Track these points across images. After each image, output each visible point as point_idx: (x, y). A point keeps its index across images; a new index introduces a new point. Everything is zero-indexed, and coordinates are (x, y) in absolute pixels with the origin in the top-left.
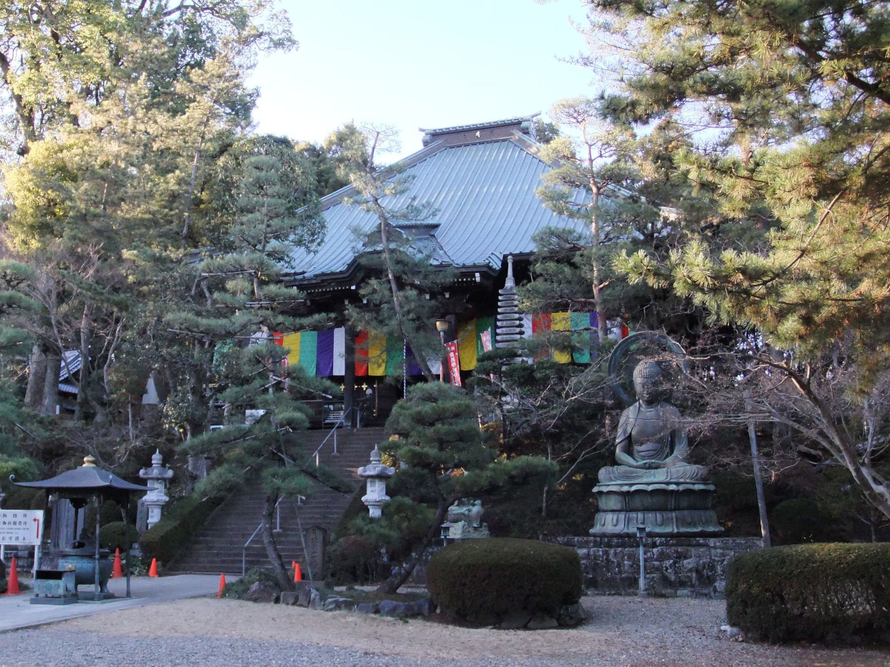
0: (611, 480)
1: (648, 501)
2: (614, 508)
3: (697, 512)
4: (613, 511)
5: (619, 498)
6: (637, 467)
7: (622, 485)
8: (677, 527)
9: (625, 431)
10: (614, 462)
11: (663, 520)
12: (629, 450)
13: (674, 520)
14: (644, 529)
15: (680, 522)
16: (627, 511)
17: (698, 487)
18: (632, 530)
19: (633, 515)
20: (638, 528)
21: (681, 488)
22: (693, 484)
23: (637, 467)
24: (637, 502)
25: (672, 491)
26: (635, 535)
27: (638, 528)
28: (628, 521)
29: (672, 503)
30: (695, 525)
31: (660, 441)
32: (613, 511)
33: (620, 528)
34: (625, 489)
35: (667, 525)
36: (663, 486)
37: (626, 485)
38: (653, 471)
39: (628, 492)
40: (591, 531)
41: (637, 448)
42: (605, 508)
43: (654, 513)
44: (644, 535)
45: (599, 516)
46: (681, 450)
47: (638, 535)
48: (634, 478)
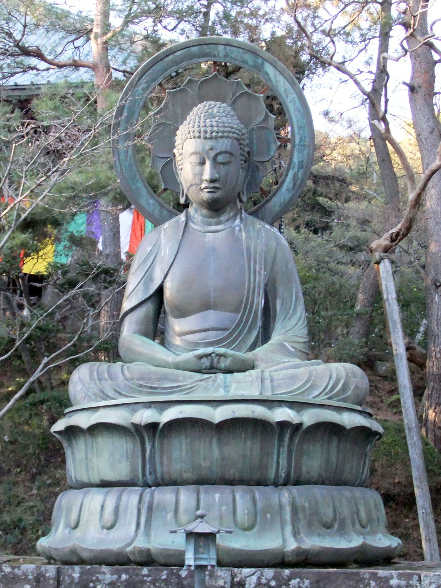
0: (107, 397)
1: (211, 454)
2: (111, 476)
3: (346, 492)
4: (105, 484)
6: (177, 366)
7: (133, 406)
8: (296, 534)
9: (148, 277)
10: (111, 351)
11: (255, 514)
12: (156, 330)
13: (288, 516)
14: (210, 537)
15: (306, 518)
16: (146, 485)
17: (350, 420)
18: (165, 539)
19: (165, 496)
21: (308, 417)
22: (339, 409)
23: (177, 366)
24: (179, 455)
25: (283, 425)
26: (175, 561)
27: (190, 535)
28: (150, 513)
29: (279, 462)
30: (342, 530)
31: (240, 306)
32: (105, 484)
33: (124, 537)
34: (145, 416)
35: (267, 526)
36: (258, 411)
37: (149, 405)
38: (221, 376)
39: (153, 427)
40: (43, 543)
41: (177, 325)
42: (85, 479)
43: (227, 489)
44: (209, 559)
45: (67, 502)
46: (291, 327)
47: (190, 560)
48: (172, 390)
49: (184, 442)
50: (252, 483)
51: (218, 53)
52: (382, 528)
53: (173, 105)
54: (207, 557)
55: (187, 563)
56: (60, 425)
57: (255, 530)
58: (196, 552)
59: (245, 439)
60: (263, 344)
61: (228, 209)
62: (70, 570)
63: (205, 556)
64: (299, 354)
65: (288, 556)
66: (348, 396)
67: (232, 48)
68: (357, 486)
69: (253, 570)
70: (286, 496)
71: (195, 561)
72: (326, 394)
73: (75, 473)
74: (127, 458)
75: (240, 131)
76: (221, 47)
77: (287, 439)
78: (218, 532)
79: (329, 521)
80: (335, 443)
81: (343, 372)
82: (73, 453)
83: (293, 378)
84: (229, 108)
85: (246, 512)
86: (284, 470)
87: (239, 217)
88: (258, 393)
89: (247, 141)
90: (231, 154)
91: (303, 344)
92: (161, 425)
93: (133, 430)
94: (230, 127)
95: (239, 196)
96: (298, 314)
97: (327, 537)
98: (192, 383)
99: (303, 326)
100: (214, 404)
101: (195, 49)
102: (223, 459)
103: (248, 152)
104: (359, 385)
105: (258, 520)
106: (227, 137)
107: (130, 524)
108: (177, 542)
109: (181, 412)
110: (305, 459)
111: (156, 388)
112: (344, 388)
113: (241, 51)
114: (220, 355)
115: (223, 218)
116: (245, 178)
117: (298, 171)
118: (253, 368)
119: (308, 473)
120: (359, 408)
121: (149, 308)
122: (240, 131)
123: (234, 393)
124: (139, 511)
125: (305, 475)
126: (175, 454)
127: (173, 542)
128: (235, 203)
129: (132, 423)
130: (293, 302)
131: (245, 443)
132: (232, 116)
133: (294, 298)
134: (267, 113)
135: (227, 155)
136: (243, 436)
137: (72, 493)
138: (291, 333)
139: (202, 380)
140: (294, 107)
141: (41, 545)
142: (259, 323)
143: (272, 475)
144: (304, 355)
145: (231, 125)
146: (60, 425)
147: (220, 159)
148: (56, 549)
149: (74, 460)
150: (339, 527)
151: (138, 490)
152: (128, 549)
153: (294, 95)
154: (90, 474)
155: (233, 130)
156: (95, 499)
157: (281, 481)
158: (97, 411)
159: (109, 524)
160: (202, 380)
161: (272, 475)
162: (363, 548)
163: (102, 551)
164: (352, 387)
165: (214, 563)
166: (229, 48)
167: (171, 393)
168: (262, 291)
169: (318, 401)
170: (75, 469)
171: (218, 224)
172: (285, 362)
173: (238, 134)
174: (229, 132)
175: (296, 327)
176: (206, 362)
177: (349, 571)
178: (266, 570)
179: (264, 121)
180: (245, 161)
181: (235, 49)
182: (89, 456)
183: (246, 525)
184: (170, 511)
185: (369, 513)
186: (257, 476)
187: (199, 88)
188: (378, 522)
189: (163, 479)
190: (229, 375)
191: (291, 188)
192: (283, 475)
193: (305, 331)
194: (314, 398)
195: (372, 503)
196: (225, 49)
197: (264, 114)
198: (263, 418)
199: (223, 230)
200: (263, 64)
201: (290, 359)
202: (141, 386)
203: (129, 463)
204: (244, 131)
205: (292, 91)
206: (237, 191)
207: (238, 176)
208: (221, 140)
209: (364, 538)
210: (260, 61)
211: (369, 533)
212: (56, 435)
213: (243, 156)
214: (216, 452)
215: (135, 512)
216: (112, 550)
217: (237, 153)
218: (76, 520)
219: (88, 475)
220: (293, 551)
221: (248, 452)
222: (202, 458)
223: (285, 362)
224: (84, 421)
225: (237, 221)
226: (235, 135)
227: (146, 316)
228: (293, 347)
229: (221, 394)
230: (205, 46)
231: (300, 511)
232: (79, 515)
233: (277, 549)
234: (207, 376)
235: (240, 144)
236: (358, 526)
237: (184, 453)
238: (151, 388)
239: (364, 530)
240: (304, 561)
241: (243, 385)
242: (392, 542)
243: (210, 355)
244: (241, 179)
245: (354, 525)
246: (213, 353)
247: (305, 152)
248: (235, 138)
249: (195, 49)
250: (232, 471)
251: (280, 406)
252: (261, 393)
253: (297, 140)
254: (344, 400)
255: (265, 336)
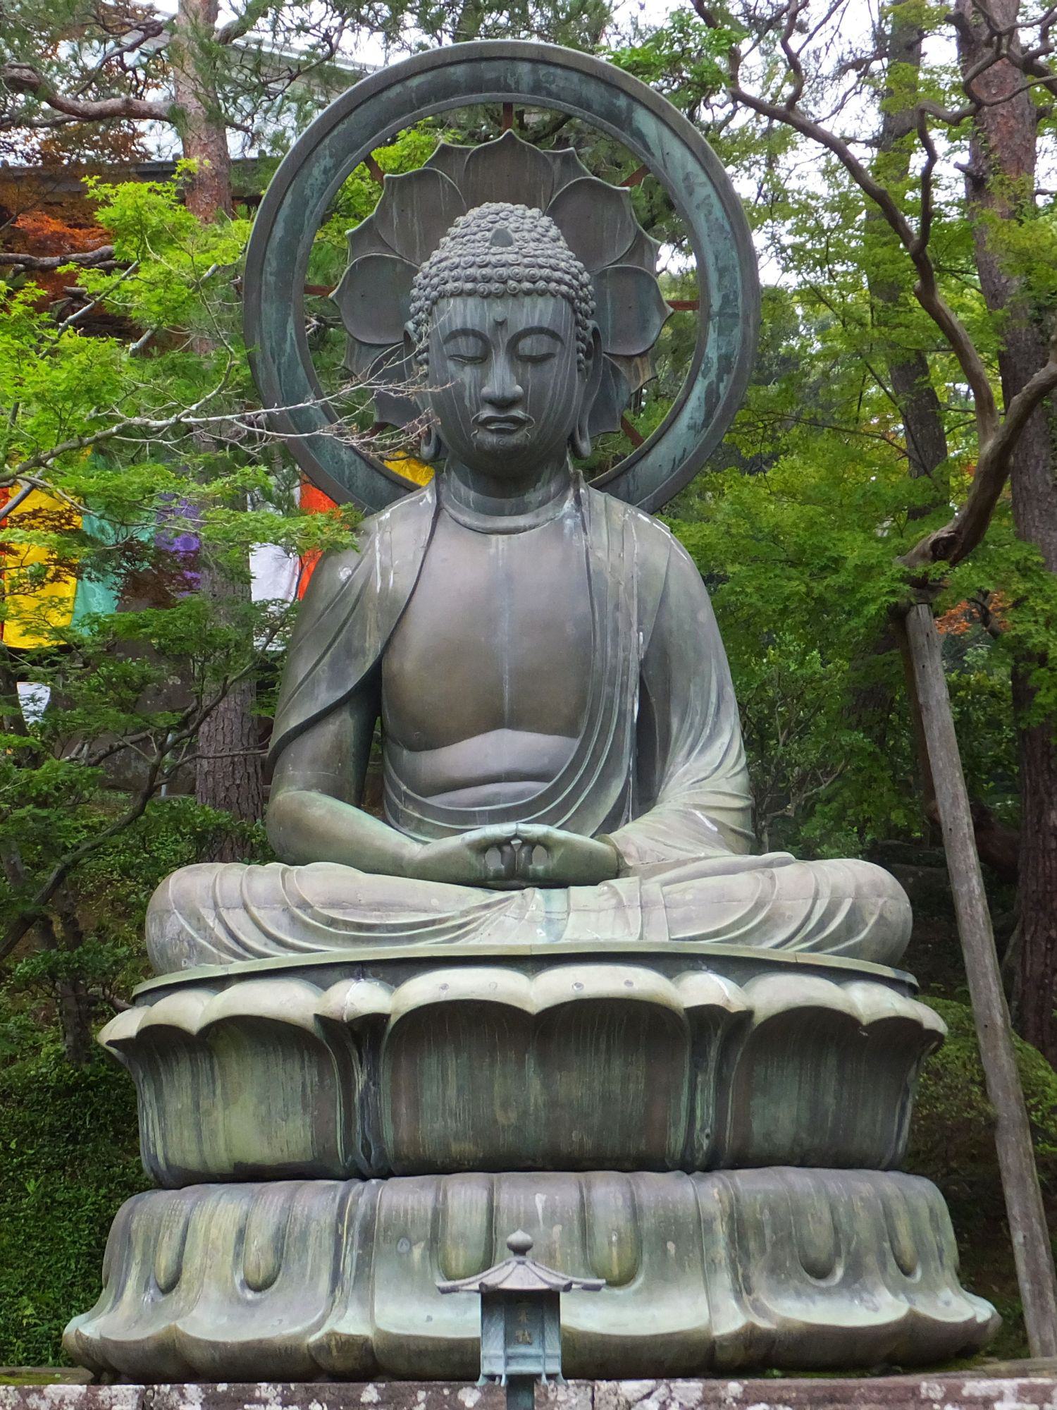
1: (525, 1094)
2: (258, 1151)
5: (294, 1076)
8: (743, 1288)
14: (543, 1304)
17: (871, 1001)
19: (404, 1197)
20: (494, 1300)
21: (771, 995)
22: (840, 976)
24: (441, 1100)
25: (707, 1017)
26: (456, 1363)
29: (697, 1110)
30: (856, 1279)
35: (666, 1275)
36: (642, 982)
37: (358, 969)
39: (374, 1022)
40: (86, 1327)
44: (542, 1358)
46: (709, 771)
49: (452, 1064)
50: (627, 1165)
51: (517, 83)
52: (949, 1275)
53: (402, 211)
54: (540, 1352)
55: (486, 1369)
56: (125, 1025)
57: (640, 1280)
58: (509, 1340)
59: (608, 1050)
60: (636, 815)
61: (546, 475)
62: (176, 1395)
63: (531, 1351)
64: (732, 838)
65: (721, 1347)
66: (860, 943)
67: (552, 70)
68: (886, 1170)
69: (649, 1384)
70: (709, 1194)
71: (507, 1364)
72: (805, 939)
73: (165, 1146)
74: (305, 1107)
75: (575, 277)
76: (524, 68)
77: (713, 1053)
78: (568, 1288)
79: (823, 1257)
80: (832, 1061)
81: (855, 883)
82: (159, 1095)
83: (723, 901)
84: (546, 221)
85: (614, 1238)
86: (708, 1131)
87: (571, 493)
88: (634, 938)
89: (593, 304)
90: (553, 335)
91: (740, 814)
92: (393, 1020)
93: (319, 1034)
94: (551, 267)
95: (572, 440)
96: (724, 739)
97: (817, 1297)
98: (465, 913)
99: (738, 768)
100: (149, 997)
101: (459, 71)
102: (552, 1104)
103: (595, 333)
104: (888, 915)
105: (646, 1258)
106: (542, 293)
107: (316, 1271)
108: (457, 1319)
109: (445, 987)
110: (758, 1102)
111: (370, 928)
112: (850, 927)
113: (575, 77)
114: (531, 843)
115: (533, 496)
116: (587, 396)
117: (720, 379)
118: (617, 874)
119: (767, 1136)
120: (888, 972)
121: (344, 726)
122: (575, 277)
123: (577, 935)
124: (338, 1239)
125: (758, 1141)
126: (430, 1094)
127: (429, 1319)
128: (562, 461)
129: (316, 1016)
130: (712, 710)
131: (608, 1061)
132: (555, 240)
133: (714, 699)
134: (639, 234)
135: (546, 338)
136: (603, 1047)
137: (158, 1202)
138: (708, 786)
139: (487, 906)
140: (707, 221)
141: (79, 1336)
142: (627, 762)
143: (676, 1141)
144: (743, 842)
145: (552, 261)
146: (125, 1025)
147: (526, 346)
148: (118, 1345)
149: (162, 1113)
150: (846, 1274)
151: (335, 1186)
152: (313, 1339)
153: (709, 190)
154: (206, 1147)
155: (558, 274)
156: (221, 1210)
157: (700, 1157)
158: (222, 989)
159: (259, 1279)
160: (487, 906)
161: (676, 1141)
162: (912, 1328)
163: (246, 1346)
164: (872, 921)
165: (555, 1367)
166: (543, 70)
167: (411, 939)
168: (633, 680)
169: (788, 954)
170: (164, 1137)
171: (521, 511)
172: (699, 859)
173: (570, 286)
174: (548, 280)
175: (720, 772)
176: (494, 862)
177: (769, 1382)
178: (680, 1384)
179: (631, 253)
180: (588, 355)
181: (559, 71)
182: (204, 1104)
183: (616, 1271)
184: (419, 1240)
185: (917, 1235)
186: (640, 1145)
187: (467, 169)
188: (941, 1258)
189: (398, 1158)
190: (557, 893)
191: (700, 422)
192: (705, 1143)
193: (742, 779)
194: (777, 946)
195: (925, 1213)
196: (534, 72)
197: (632, 234)
198: (657, 1000)
199: (531, 528)
200: (630, 111)
201: (710, 852)
202: (332, 922)
203: (308, 1120)
204: (585, 277)
205: (702, 178)
206: (566, 431)
207: (571, 388)
208: (527, 300)
209: (910, 1301)
210: (622, 102)
211: (918, 1288)
212: (113, 1050)
213: (583, 340)
214: (535, 1085)
215: (328, 1242)
216: (269, 1341)
217: (568, 333)
218: (173, 1268)
219: (201, 1152)
220: (736, 1336)
221: (616, 1088)
222: (497, 1102)
223: (699, 859)
224: (193, 1011)
225: (568, 505)
226: (564, 288)
227: (338, 747)
228: (714, 821)
229: (538, 940)
230: (483, 65)
231: (750, 1233)
232: (180, 1255)
233: (697, 1331)
234: (499, 895)
235: (575, 311)
236: (892, 1267)
237: (452, 1092)
238: (360, 927)
239: (908, 1280)
240: (759, 1357)
241: (586, 916)
242: (977, 1309)
243: (507, 841)
244: (577, 400)
245: (883, 1266)
246: (516, 837)
247: (737, 332)
248: (565, 296)
249: (459, 71)
250: (575, 1136)
251: (696, 969)
252: (641, 937)
253: (716, 302)
254: (850, 952)
255: (644, 794)
